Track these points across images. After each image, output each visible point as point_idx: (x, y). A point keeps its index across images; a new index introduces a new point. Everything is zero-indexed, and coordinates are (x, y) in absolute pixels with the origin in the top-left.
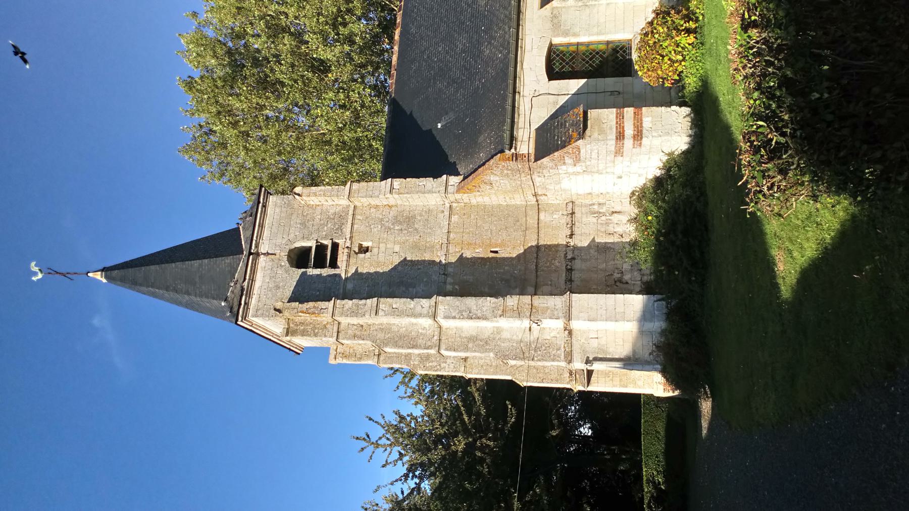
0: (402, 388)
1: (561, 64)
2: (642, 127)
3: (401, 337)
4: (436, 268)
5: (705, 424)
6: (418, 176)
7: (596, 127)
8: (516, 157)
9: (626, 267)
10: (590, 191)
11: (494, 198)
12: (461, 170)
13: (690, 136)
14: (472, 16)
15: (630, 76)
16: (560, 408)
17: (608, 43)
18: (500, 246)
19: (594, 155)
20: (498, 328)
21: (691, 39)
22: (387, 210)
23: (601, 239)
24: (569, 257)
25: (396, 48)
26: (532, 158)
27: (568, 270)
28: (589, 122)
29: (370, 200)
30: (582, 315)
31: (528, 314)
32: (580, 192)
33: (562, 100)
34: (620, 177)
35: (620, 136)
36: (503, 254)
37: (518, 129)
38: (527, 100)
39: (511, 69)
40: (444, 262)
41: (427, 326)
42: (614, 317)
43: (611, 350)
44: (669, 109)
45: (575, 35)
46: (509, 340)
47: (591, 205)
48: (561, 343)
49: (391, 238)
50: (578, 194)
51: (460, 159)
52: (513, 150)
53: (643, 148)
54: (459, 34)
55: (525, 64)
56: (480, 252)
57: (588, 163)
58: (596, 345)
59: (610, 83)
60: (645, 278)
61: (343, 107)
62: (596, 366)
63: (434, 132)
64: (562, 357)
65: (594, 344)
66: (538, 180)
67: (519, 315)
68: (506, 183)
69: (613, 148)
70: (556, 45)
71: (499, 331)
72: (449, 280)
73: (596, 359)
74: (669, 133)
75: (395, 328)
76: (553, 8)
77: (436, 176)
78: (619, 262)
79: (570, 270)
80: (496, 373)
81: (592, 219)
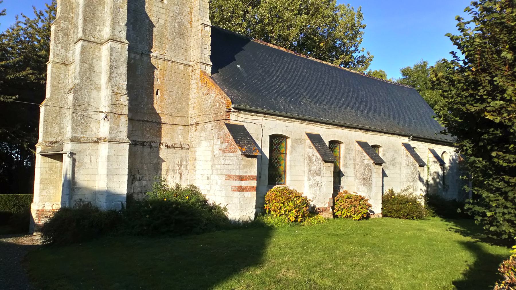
0: (23, 20)
1: (277, 143)
2: (246, 191)
3: (93, 12)
4: (147, 48)
5: (11, 240)
6: (212, 45)
7: (247, 163)
8: (229, 111)
9: (144, 183)
10: (197, 159)
11: (195, 96)
12: (215, 75)
13: (239, 221)
14: (297, 94)
15: (269, 184)
16: (11, 136)
18: (162, 97)
19: (227, 162)
20: (100, 88)
21: (292, 219)
23: (164, 166)
24: (152, 144)
25: (276, 47)
26: (227, 122)
27: (143, 143)
29: (197, 8)
30: (113, 151)
31: (114, 111)
32: (197, 154)
33: (259, 143)
34: (208, 179)
35: (242, 178)
36: (156, 98)
38: (260, 121)
39: (278, 113)
40: (152, 54)
41: (102, 33)
42: (110, 174)
43: (81, 171)
44: (254, 207)
45: (291, 152)
46: (90, 96)
47: (186, 160)
48: (87, 135)
49: (169, 19)
50: (195, 152)
52: (233, 110)
53: (231, 192)
54: (287, 85)
55: (279, 121)
56: (158, 82)
58: (85, 160)
59: (266, 172)
60: (135, 196)
61: (233, 12)
62: (67, 160)
63: (234, 62)
64: (76, 135)
65: (87, 159)
66: (210, 125)
67: (114, 104)
68: (208, 104)
70: (286, 141)
71: (98, 89)
72: (138, 57)
73: (74, 160)
74: (240, 209)
75: (100, 8)
76: (305, 140)
77: (212, 58)
79: (143, 144)
80: (52, 85)
81: (177, 160)
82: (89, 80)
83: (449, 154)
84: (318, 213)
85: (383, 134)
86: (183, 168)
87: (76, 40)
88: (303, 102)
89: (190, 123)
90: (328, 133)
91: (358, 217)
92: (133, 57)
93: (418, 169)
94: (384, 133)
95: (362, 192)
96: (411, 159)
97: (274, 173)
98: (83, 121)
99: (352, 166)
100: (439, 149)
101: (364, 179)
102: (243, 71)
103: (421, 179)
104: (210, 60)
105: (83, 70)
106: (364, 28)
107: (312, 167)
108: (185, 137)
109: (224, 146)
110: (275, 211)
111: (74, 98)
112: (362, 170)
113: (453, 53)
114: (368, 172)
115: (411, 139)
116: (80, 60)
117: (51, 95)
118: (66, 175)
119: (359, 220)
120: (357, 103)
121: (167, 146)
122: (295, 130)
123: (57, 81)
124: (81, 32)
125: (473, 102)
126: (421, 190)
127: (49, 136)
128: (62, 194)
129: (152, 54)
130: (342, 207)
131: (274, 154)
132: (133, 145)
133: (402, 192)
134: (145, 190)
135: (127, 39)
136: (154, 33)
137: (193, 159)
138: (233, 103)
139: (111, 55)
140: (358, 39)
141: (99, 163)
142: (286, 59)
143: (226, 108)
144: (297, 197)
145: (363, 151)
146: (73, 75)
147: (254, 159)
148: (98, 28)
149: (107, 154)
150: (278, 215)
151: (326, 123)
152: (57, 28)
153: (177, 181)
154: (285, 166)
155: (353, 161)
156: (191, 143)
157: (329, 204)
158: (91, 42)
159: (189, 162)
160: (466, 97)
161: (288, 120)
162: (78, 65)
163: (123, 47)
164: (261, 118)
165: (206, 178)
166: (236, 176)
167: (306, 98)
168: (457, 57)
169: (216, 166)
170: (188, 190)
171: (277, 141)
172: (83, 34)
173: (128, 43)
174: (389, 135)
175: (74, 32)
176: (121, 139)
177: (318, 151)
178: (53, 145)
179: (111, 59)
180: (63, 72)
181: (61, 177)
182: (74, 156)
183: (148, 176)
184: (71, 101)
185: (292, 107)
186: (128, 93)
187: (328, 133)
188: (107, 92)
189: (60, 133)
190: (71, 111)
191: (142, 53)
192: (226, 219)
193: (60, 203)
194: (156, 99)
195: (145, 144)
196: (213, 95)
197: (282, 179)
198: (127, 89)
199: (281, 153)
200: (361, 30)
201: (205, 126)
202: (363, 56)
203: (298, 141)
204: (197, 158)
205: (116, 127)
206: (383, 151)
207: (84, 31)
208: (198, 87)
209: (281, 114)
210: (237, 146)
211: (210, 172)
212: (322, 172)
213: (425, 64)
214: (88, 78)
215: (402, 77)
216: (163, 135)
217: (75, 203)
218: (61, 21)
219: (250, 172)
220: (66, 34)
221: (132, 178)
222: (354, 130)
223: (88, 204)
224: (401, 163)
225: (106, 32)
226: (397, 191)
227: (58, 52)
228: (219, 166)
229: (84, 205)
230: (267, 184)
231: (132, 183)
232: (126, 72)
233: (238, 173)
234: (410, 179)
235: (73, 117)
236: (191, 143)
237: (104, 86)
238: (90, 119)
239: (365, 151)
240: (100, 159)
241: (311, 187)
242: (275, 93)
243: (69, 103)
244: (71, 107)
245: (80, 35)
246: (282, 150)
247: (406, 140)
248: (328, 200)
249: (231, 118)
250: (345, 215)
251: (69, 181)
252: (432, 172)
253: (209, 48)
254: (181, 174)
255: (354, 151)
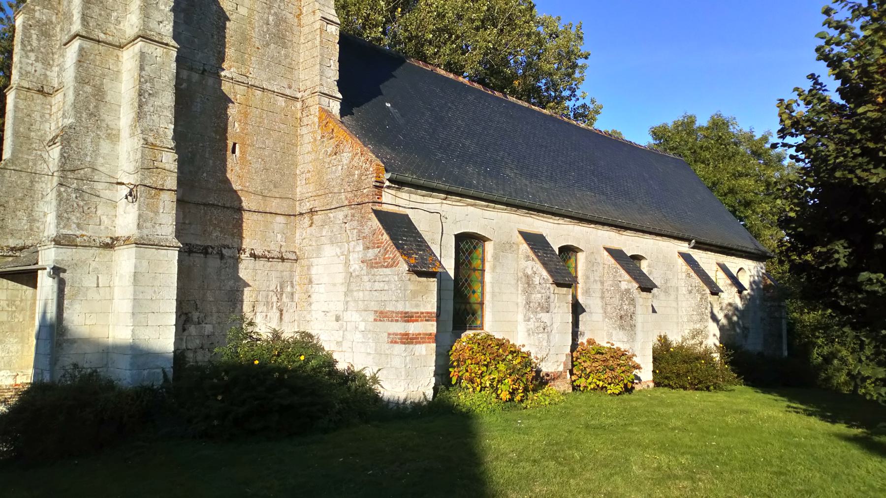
1: (467, 250)
2: (417, 343)
4: (213, 61)
6: (341, 60)
7: (419, 288)
8: (379, 187)
9: (208, 329)
10: (315, 281)
11: (309, 158)
13: (405, 400)
15: (454, 328)
17: (482, 304)
19: (378, 286)
20: (117, 136)
21: (505, 396)
22: (295, 11)
23: (248, 295)
24: (224, 251)
26: (377, 207)
28: (425, 279)
30: (145, 263)
31: (146, 182)
32: (314, 271)
33: (435, 249)
34: (338, 319)
35: (408, 317)
37: (410, 193)
38: (437, 208)
40: (223, 74)
41: (121, 26)
44: (432, 374)
45: (494, 268)
46: (96, 152)
50: (309, 267)
51: (357, 121)
52: (387, 183)
53: (387, 346)
56: (235, 128)
57: (366, 278)
58: (86, 283)
59: (450, 306)
60: (190, 355)
63: (380, 97)
64: (65, 231)
65: (89, 282)
66: (340, 215)
67: (148, 167)
69: (390, 308)
70: (483, 246)
71: (113, 137)
72: (196, 77)
73: (61, 284)
74: (404, 377)
78: (214, 319)
80: (16, 134)
82: (93, 119)
83: (748, 273)
84: (546, 383)
85: (647, 236)
86: (285, 299)
87: (66, 38)
88: (508, 175)
89: (298, 210)
90: (558, 232)
91: (618, 389)
92: (185, 77)
93: (709, 299)
94: (651, 233)
95: (620, 342)
96: (696, 280)
97: (463, 307)
98: (81, 203)
99: (598, 294)
100: (734, 263)
101: (621, 317)
102: (398, 115)
103: (714, 318)
104: (336, 89)
105: (81, 98)
106: (586, 58)
107: (533, 296)
108: (289, 239)
109: (371, 254)
110: (472, 381)
111: (62, 155)
112: (616, 301)
113: (812, 76)
114: (629, 304)
115: (692, 245)
116: (76, 78)
117: (13, 153)
118: (44, 313)
119: (620, 394)
120: (596, 180)
121: (254, 256)
122: (498, 224)
123: (27, 125)
124: (79, 21)
125: (871, 166)
126: (714, 335)
127: (9, 236)
128: (36, 353)
129: (223, 74)
130: (588, 370)
131: (462, 271)
132: (187, 252)
133: (684, 339)
134: (209, 343)
135: (175, 38)
136: (229, 32)
137: (306, 282)
138: (387, 171)
139: (142, 68)
140: (577, 75)
141: (116, 289)
142: (469, 97)
143: (374, 179)
144: (512, 352)
145: (619, 266)
146: (58, 113)
147: (432, 279)
148: (114, 14)
149: (133, 271)
150: (478, 389)
151: (554, 214)
152: (28, 20)
153: (274, 324)
154: (483, 294)
155: (599, 283)
156: (300, 250)
157: (565, 364)
158: (99, 41)
159: (297, 287)
160: (856, 156)
161: (487, 206)
162: (72, 89)
163: (167, 53)
164: (440, 201)
165: (334, 318)
166: (397, 313)
167: (511, 169)
168: (821, 84)
169: (355, 294)
170: (295, 342)
171: (468, 244)
172: (83, 25)
173: (176, 45)
174: (658, 238)
175: (62, 30)
176: (160, 240)
177: (545, 265)
178: (18, 254)
179: (140, 76)
180: (38, 108)
181: (33, 318)
182: (62, 275)
183: (215, 315)
184: (56, 161)
185: (491, 183)
186: (176, 146)
187: (558, 232)
188: (132, 142)
189: (31, 230)
190: (55, 180)
191: (204, 70)
192: (376, 399)
193: (31, 371)
194: (233, 162)
195: (210, 250)
196: (346, 157)
197: (476, 318)
198: (175, 138)
199: (475, 270)
200: (580, 62)
201: (331, 215)
202: (584, 106)
203: (506, 247)
204: (313, 280)
205: (152, 215)
206: (649, 266)
207: (84, 18)
208: (315, 140)
209: (476, 194)
210: (398, 254)
211: (341, 306)
212: (552, 305)
213: (691, 120)
214: (91, 115)
215: (652, 142)
216: (245, 233)
217: (62, 372)
218: (37, 8)
219: (425, 306)
220: (45, 31)
221: (185, 318)
222: (600, 227)
223: (91, 375)
224: (677, 288)
225: (131, 23)
226: (675, 339)
227: (29, 68)
228: (361, 294)
229: (82, 377)
230: (451, 329)
231: (184, 330)
232: (173, 104)
233: (400, 307)
234: (695, 318)
235: (59, 194)
236: (300, 250)
237: (125, 132)
238: (96, 199)
239: (622, 266)
240: (117, 281)
241: (530, 333)
242: (458, 157)
243: (51, 165)
244: (55, 174)
245: (76, 26)
246: (476, 263)
247: (684, 247)
248: (564, 358)
249: (384, 200)
250: (592, 386)
251: (51, 326)
252: (724, 305)
253: (335, 65)
254: (281, 311)
255: (602, 266)
